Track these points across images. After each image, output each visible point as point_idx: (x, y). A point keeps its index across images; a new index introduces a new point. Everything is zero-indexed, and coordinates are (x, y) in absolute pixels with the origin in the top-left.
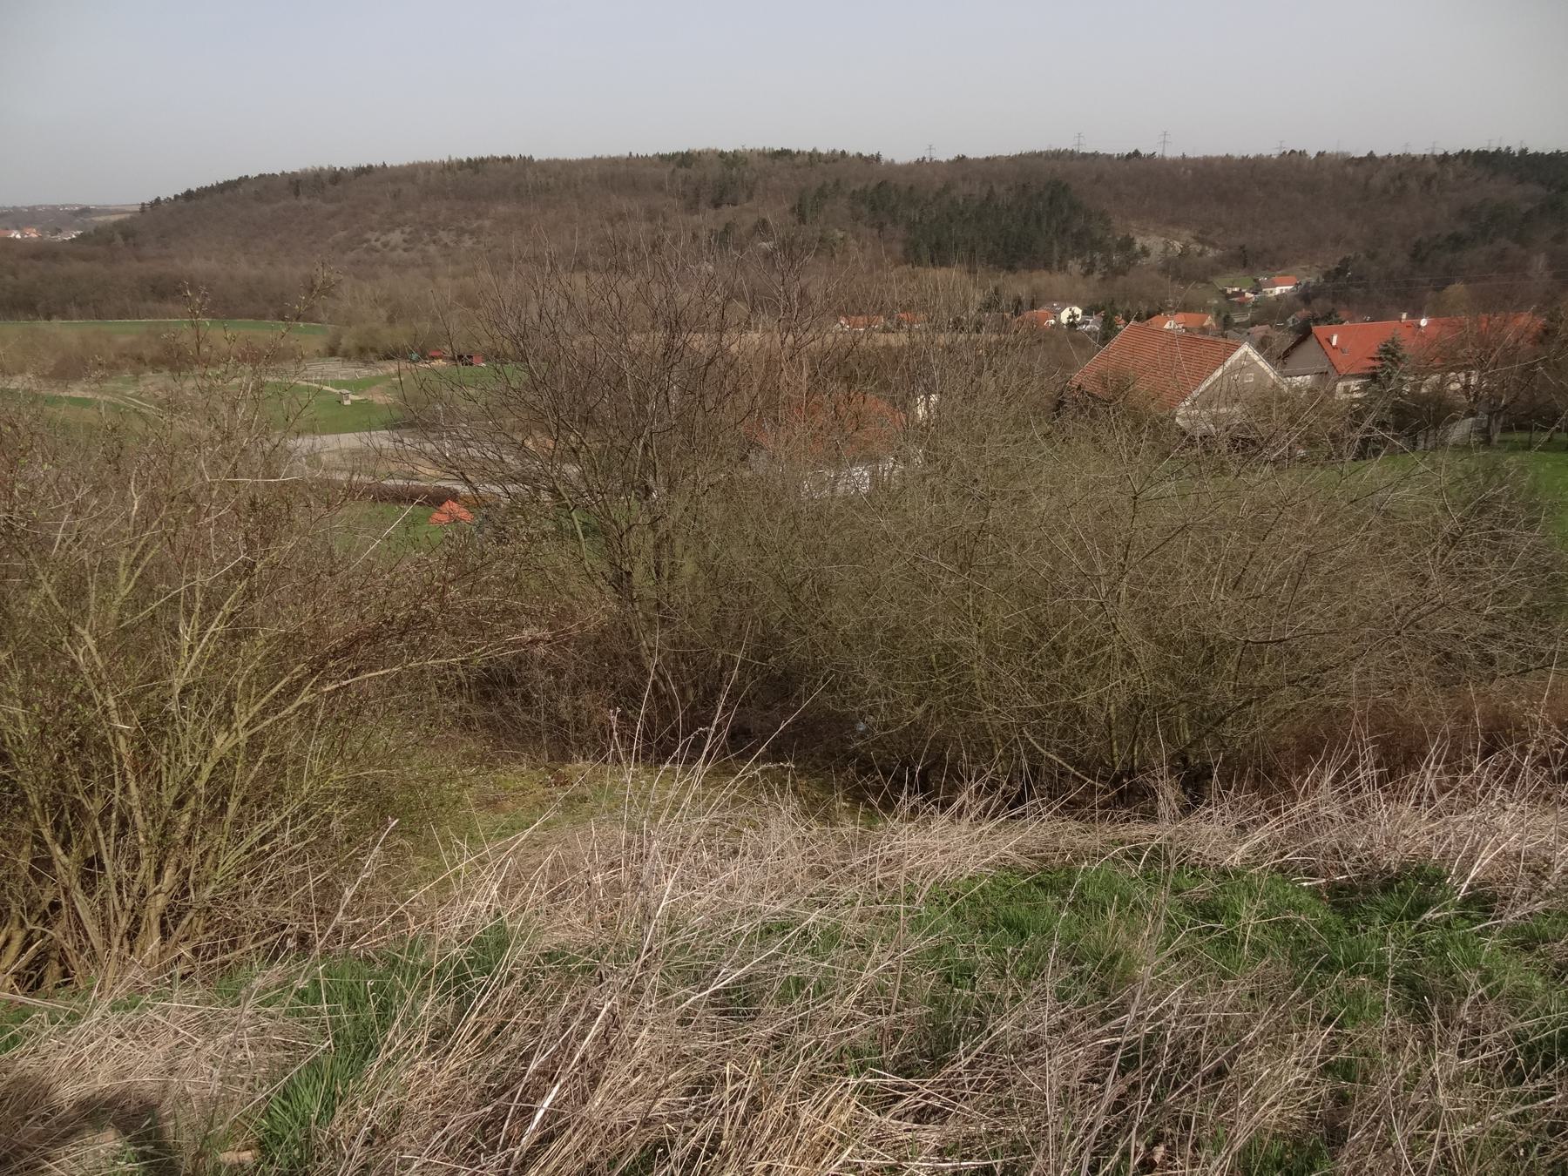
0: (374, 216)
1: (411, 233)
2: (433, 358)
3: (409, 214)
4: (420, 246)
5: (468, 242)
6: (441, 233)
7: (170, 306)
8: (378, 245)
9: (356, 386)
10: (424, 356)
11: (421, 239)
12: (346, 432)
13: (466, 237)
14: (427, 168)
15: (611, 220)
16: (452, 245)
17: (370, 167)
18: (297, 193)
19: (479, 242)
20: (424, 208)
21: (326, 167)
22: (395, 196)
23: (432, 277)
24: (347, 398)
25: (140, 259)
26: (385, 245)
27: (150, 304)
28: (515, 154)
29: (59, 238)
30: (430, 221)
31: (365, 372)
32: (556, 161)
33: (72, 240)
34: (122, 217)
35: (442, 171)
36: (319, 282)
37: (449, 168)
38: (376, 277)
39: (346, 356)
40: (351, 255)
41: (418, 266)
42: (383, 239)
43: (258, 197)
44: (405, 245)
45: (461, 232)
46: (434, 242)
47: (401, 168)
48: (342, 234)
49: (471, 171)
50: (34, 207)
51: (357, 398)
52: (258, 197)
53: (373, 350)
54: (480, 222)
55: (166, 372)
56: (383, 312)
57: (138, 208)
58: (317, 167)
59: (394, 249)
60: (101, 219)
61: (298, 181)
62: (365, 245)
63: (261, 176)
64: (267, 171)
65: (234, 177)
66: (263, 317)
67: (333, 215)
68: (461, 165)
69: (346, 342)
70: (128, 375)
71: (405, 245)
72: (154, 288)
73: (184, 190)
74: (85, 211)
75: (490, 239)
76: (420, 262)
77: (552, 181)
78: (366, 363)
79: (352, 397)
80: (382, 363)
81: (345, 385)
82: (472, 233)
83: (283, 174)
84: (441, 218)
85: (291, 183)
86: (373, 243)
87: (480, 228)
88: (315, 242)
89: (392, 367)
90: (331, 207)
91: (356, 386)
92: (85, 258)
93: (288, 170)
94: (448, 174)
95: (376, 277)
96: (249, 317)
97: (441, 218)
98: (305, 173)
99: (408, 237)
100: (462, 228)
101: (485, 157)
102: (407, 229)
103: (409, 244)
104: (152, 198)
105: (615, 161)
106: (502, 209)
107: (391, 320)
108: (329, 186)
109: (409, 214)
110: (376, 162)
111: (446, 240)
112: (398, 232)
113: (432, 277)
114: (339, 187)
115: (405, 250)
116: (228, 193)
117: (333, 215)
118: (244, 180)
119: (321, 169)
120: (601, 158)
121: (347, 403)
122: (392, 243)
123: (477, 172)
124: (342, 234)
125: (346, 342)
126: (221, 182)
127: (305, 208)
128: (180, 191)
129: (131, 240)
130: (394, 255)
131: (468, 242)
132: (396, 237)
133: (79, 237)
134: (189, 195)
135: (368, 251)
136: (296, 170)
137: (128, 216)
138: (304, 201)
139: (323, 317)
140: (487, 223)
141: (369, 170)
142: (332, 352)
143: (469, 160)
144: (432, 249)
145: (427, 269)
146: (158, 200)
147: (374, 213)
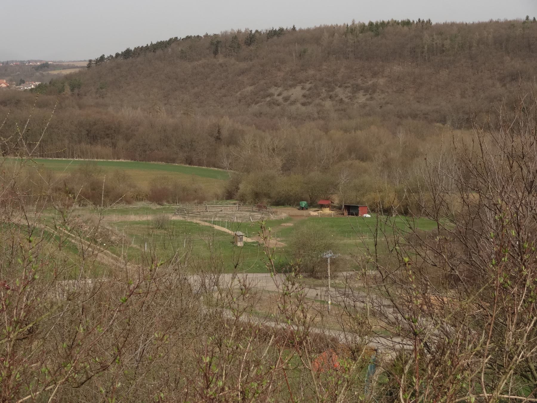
0: (279, 74)
1: (310, 89)
2: (322, 206)
3: (311, 72)
4: (317, 101)
5: (362, 98)
6: (338, 90)
7: (99, 148)
8: (280, 99)
9: (249, 229)
10: (312, 204)
11: (319, 95)
12: (250, 273)
13: (361, 94)
14: (332, 31)
15: (502, 80)
16: (346, 100)
17: (281, 30)
18: (216, 53)
19: (372, 98)
20: (324, 67)
21: (243, 30)
22: (301, 55)
23: (326, 130)
24: (241, 240)
25: (80, 107)
26: (286, 99)
27: (83, 145)
28: (414, 18)
29: (23, 87)
30: (330, 79)
31: (258, 216)
32: (453, 24)
33: (32, 90)
34: (67, 72)
35: (345, 34)
36: (225, 133)
37: (351, 30)
38: (275, 128)
39: (243, 200)
40: (255, 108)
41: (314, 119)
42: (285, 94)
43: (183, 56)
44: (304, 100)
45: (356, 89)
46: (331, 97)
47: (308, 31)
48: (249, 89)
49: (372, 34)
50: (7, 63)
51: (249, 240)
52: (183, 56)
53: (268, 196)
54: (375, 80)
55: (91, 206)
56: (279, 161)
57: (85, 64)
58: (236, 30)
59: (294, 103)
60: (56, 72)
61: (218, 42)
62: (268, 99)
63: (188, 38)
64: (194, 33)
65: (166, 38)
66: (173, 161)
67: (243, 72)
68: (363, 28)
69: (244, 187)
70: (59, 205)
71: (304, 100)
72: (89, 132)
73: (124, 50)
74: (45, 66)
75: (383, 96)
76: (316, 115)
77: (447, 43)
78: (260, 208)
79: (245, 239)
80: (274, 209)
81: (238, 227)
82: (366, 90)
83: (206, 36)
84: (339, 76)
85: (212, 44)
86: (275, 97)
87: (375, 86)
88: (225, 96)
89: (284, 213)
90: (243, 65)
91: (249, 229)
92: (41, 105)
93: (211, 33)
94: (350, 36)
95: (275, 128)
96: (161, 160)
97: (339, 76)
98: (225, 35)
99: (307, 93)
100: (357, 85)
101: (386, 20)
102: (308, 86)
103: (306, 102)
104: (98, 56)
105: (511, 25)
106: (397, 69)
107: (286, 168)
108: (244, 47)
109: (311, 72)
110: (287, 25)
111: (342, 96)
112: (299, 88)
113: (326, 130)
114: (252, 48)
115: (303, 104)
116: (159, 52)
117: (243, 72)
118: (174, 41)
119: (239, 32)
120: (497, 22)
121: (239, 244)
122: (293, 98)
123: (377, 35)
124: (249, 89)
125: (244, 187)
126: (154, 42)
127: (221, 65)
128: (121, 49)
129: (76, 91)
130: (293, 108)
131: (362, 98)
132: (297, 92)
133: (38, 87)
134: (127, 54)
135: (270, 104)
136: (218, 32)
137: (77, 70)
138: (221, 59)
139: (226, 163)
140: (381, 81)
141: (280, 33)
142: (229, 196)
143: (371, 24)
144: (328, 104)
145: (322, 122)
146: (102, 58)
147: (279, 70)
